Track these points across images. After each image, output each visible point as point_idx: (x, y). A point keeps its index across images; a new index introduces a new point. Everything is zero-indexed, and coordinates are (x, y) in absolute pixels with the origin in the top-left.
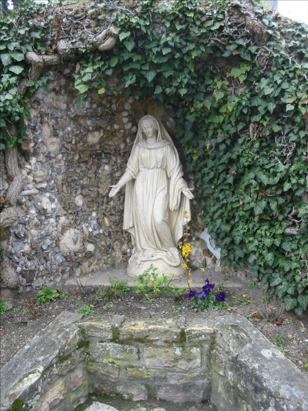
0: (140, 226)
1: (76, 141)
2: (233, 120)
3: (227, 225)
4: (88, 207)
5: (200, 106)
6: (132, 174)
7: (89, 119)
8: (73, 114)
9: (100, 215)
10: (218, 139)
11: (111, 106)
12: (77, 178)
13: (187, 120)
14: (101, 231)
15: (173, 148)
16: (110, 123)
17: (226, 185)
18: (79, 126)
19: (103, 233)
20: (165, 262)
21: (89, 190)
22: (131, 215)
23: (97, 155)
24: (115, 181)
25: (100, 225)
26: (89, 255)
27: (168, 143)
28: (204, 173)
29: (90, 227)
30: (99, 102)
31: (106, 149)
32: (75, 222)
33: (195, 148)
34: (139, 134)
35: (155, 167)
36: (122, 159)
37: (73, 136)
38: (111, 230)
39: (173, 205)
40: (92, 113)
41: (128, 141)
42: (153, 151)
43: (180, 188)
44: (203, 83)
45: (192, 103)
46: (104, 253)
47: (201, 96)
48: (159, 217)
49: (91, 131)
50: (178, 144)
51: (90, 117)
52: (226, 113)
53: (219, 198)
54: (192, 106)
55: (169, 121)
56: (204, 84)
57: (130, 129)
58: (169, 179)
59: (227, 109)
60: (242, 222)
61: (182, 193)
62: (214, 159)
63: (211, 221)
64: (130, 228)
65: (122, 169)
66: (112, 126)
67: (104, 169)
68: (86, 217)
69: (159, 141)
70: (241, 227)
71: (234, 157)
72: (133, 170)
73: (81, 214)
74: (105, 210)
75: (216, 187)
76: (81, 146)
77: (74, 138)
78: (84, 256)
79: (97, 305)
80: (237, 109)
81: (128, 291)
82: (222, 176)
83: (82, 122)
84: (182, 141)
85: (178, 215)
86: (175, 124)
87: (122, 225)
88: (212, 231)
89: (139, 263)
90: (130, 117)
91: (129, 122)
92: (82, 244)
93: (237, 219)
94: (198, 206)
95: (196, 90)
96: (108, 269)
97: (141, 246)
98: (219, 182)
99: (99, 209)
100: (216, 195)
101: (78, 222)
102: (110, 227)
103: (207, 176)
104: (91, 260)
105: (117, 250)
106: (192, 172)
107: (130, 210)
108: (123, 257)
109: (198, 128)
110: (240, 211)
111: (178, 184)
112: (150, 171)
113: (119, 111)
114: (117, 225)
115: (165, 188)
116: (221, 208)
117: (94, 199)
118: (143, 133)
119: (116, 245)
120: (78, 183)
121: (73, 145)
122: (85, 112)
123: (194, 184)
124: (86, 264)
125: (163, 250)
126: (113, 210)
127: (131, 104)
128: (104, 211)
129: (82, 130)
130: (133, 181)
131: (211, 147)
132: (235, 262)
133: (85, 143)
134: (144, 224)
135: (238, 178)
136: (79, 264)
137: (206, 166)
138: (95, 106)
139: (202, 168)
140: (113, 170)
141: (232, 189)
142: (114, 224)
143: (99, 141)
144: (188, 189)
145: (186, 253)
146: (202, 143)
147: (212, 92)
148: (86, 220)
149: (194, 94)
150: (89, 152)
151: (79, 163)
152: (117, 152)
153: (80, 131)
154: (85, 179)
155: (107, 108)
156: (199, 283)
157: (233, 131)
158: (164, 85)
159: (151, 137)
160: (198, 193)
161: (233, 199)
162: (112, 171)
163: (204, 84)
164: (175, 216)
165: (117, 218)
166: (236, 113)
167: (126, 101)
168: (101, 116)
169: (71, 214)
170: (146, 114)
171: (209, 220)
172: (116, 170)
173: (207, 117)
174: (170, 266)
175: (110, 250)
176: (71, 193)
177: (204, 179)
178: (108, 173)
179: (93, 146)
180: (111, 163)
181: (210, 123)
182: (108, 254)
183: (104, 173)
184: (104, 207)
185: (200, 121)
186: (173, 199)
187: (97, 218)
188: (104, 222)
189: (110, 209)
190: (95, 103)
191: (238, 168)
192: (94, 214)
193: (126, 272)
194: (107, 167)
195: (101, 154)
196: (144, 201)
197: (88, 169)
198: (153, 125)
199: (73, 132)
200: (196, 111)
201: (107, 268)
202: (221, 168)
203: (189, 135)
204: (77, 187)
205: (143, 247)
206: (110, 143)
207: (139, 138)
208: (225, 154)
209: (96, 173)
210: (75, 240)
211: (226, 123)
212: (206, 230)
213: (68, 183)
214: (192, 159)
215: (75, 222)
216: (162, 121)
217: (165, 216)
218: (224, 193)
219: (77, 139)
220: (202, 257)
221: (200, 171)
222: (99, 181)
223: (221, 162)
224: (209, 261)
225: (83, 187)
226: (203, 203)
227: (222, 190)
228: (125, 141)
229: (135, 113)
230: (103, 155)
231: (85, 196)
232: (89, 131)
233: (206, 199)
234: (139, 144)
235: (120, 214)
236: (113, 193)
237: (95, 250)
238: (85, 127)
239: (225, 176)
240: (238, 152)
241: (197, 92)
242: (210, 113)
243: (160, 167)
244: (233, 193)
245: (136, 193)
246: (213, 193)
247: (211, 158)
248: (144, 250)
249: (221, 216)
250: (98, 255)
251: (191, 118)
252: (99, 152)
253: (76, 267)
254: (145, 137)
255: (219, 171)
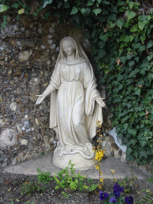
0: (62, 127)
1: (8, 59)
2: (143, 39)
3: (133, 129)
4: (21, 111)
5: (112, 25)
6: (55, 86)
7: (19, 40)
8: (4, 36)
9: (31, 117)
10: (127, 57)
11: (37, 29)
12: (10, 89)
13: (101, 40)
14: (33, 129)
15: (89, 64)
16: (38, 44)
17: (133, 96)
18: (10, 46)
19: (35, 130)
20: (82, 155)
21: (22, 98)
22: (55, 118)
23: (28, 70)
24: (42, 89)
25: (31, 124)
26: (23, 148)
27: (85, 60)
28: (114, 85)
29: (24, 126)
30: (26, 26)
31: (35, 65)
32: (10, 124)
33: (107, 64)
34: (61, 53)
35: (73, 80)
36: (49, 73)
37: (6, 54)
38: (40, 127)
39: (89, 110)
40: (20, 35)
41: (53, 58)
42: (72, 66)
43: (94, 97)
44: (115, 5)
45: (105, 23)
46: (35, 145)
47: (114, 17)
48: (77, 120)
49: (21, 50)
50: (92, 60)
51: (20, 39)
52: (136, 32)
53: (127, 106)
54: (105, 27)
55: (85, 42)
56: (117, 6)
57: (55, 49)
58: (85, 89)
59: (138, 28)
60: (147, 128)
61: (95, 101)
62: (123, 74)
63: (119, 123)
64: (55, 127)
65: (48, 80)
66: (39, 47)
67: (34, 81)
68: (19, 119)
69: (77, 59)
70: (146, 133)
71: (143, 72)
72: (56, 82)
73: (15, 117)
74: (36, 113)
75: (124, 97)
76: (13, 63)
77: (6, 56)
78: (20, 149)
79: (23, 199)
80: (149, 27)
81: (51, 181)
82: (130, 89)
83: (13, 42)
84: (96, 58)
85: (92, 119)
86: (90, 45)
87: (49, 123)
88: (120, 132)
89: (61, 156)
90: (54, 39)
91: (53, 43)
92: (16, 140)
93: (142, 126)
94: (108, 109)
95: (109, 11)
96: (39, 157)
97: (63, 142)
98: (127, 93)
99: (30, 112)
100: (124, 104)
101: (13, 124)
102: (40, 125)
103: (117, 88)
104: (25, 151)
105: (46, 142)
106: (103, 84)
107: (54, 114)
108: (50, 147)
109: (110, 47)
110: (146, 119)
111: (93, 94)
112: (70, 83)
113: (46, 34)
114: (46, 124)
115: (82, 97)
116: (128, 114)
117: (25, 105)
118: (64, 52)
119: (45, 138)
120: (12, 93)
121: (6, 61)
122: (14, 34)
123: (105, 93)
124: (21, 154)
125: (80, 146)
126: (41, 113)
127: (55, 29)
128: (34, 114)
129: (13, 50)
130: (56, 91)
131: (121, 63)
132: (139, 160)
133: (16, 60)
134: (65, 125)
135: (144, 90)
136: (16, 155)
137: (115, 79)
138: (23, 29)
139: (112, 81)
140: (41, 81)
141: (139, 100)
142: (43, 123)
143: (29, 58)
144: (100, 98)
145: (98, 158)
146: (112, 60)
147: (124, 13)
148: (20, 122)
149: (107, 15)
150: (20, 68)
151: (13, 76)
152: (45, 67)
153: (12, 50)
154: (18, 89)
155: (34, 31)
156: (108, 175)
157: (142, 49)
158: (79, 7)
159: (70, 55)
160: (109, 100)
161: (139, 109)
162: (41, 83)
163: (117, 6)
164: (90, 119)
165: (46, 118)
166: (147, 31)
167: (50, 26)
168: (29, 38)
169: (6, 117)
170: (67, 36)
171: (117, 122)
172: (43, 81)
173: (118, 37)
174: (86, 159)
175: (40, 143)
176: (6, 101)
177: (114, 90)
178: (38, 84)
179: (24, 62)
180: (39, 76)
181: (120, 42)
182: (38, 146)
183: (34, 84)
184: (34, 111)
185: (112, 41)
186: (88, 107)
187: (29, 119)
188: (35, 122)
189: (40, 112)
190: (22, 26)
191: (145, 82)
192: (26, 117)
193: (52, 161)
194: (36, 80)
195: (31, 70)
196: (65, 107)
197: (21, 81)
198: (72, 44)
199: (5, 51)
200: (108, 32)
201: (39, 156)
202: (129, 82)
203: (102, 54)
204: (12, 96)
205: (64, 143)
206: (39, 60)
207: (60, 56)
208: (133, 69)
209: (27, 84)
210: (11, 137)
211: (136, 41)
212: (114, 129)
213: (4, 93)
214: (104, 73)
215: (10, 124)
216: (80, 43)
217: (81, 120)
218: (131, 103)
219: (9, 57)
220: (110, 149)
221: (110, 83)
222: (30, 91)
223: (130, 76)
224: (116, 152)
225: (16, 96)
226: (113, 109)
227: (129, 101)
228: (51, 59)
229: (59, 36)
230: (33, 70)
231: (18, 103)
232: (19, 50)
233: (115, 105)
234: (61, 61)
235: (48, 115)
236: (39, 101)
237: (28, 144)
238: (15, 47)
239: (132, 88)
240: (147, 68)
241: (110, 13)
242: (121, 33)
243: (78, 80)
244: (139, 103)
245: (58, 102)
246: (122, 102)
247: (120, 73)
248: (65, 145)
249: (128, 121)
250: (30, 147)
251: (104, 38)
252: (29, 67)
253: (13, 158)
254: (65, 55)
255: (127, 84)
